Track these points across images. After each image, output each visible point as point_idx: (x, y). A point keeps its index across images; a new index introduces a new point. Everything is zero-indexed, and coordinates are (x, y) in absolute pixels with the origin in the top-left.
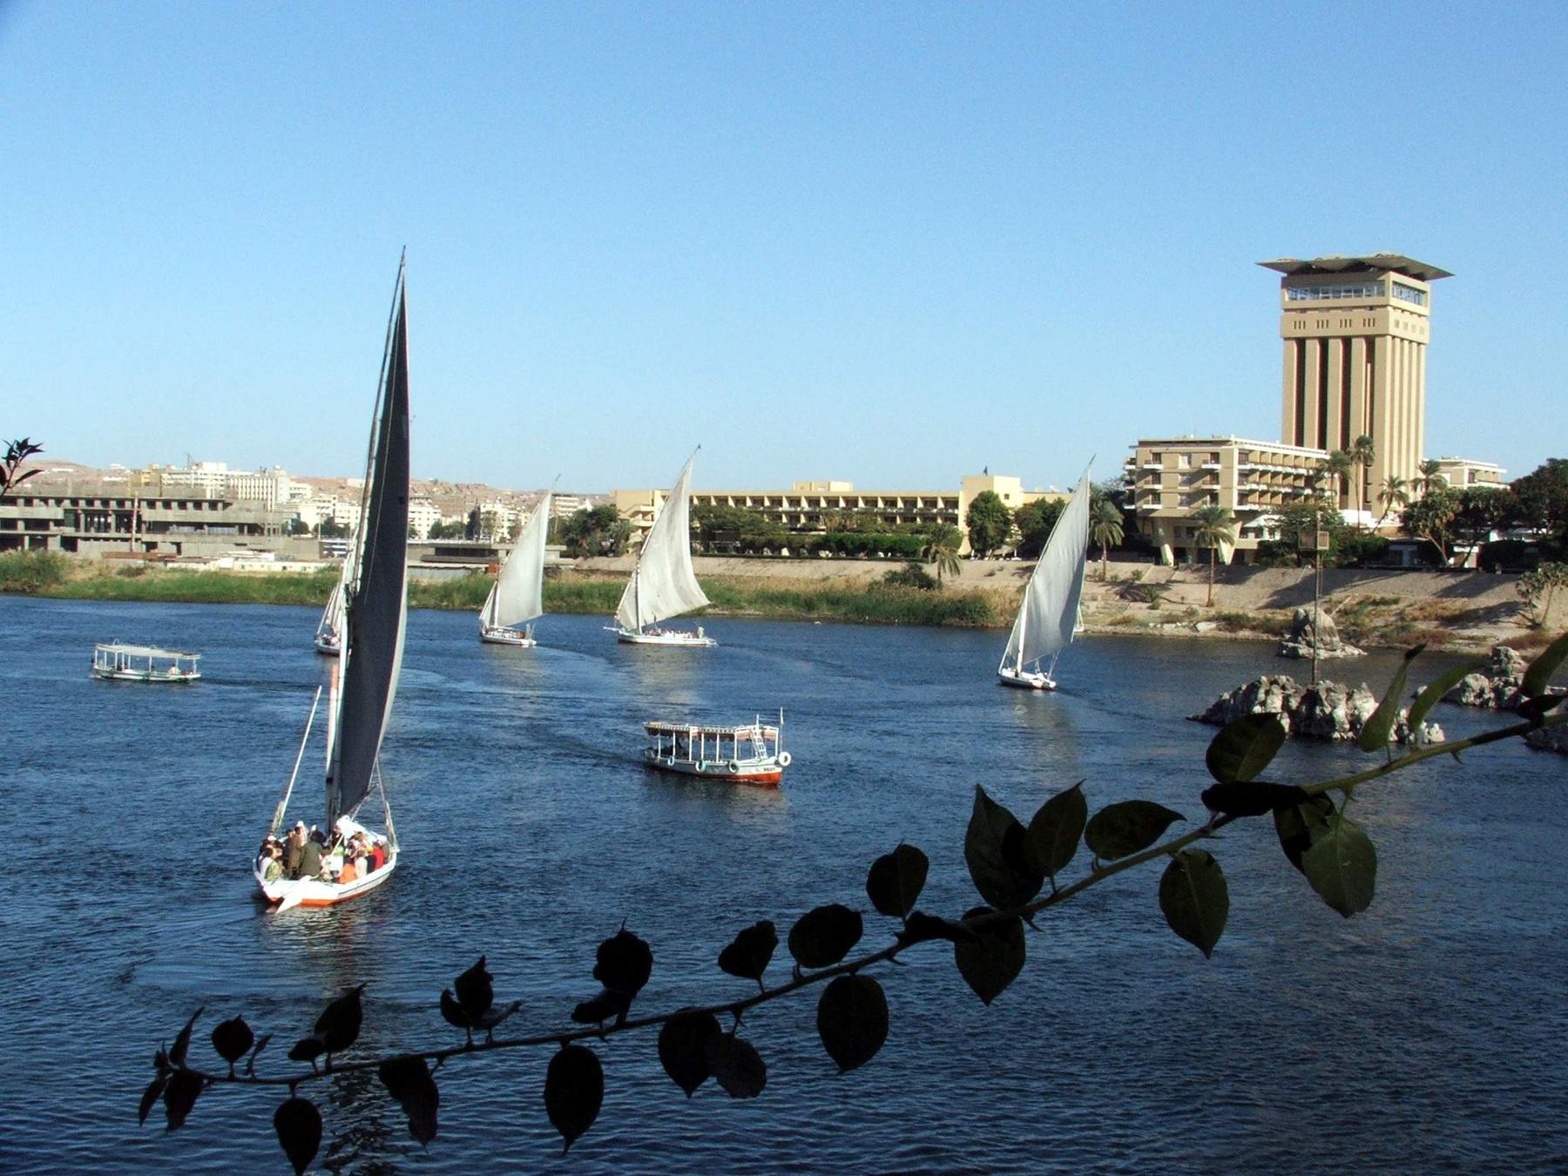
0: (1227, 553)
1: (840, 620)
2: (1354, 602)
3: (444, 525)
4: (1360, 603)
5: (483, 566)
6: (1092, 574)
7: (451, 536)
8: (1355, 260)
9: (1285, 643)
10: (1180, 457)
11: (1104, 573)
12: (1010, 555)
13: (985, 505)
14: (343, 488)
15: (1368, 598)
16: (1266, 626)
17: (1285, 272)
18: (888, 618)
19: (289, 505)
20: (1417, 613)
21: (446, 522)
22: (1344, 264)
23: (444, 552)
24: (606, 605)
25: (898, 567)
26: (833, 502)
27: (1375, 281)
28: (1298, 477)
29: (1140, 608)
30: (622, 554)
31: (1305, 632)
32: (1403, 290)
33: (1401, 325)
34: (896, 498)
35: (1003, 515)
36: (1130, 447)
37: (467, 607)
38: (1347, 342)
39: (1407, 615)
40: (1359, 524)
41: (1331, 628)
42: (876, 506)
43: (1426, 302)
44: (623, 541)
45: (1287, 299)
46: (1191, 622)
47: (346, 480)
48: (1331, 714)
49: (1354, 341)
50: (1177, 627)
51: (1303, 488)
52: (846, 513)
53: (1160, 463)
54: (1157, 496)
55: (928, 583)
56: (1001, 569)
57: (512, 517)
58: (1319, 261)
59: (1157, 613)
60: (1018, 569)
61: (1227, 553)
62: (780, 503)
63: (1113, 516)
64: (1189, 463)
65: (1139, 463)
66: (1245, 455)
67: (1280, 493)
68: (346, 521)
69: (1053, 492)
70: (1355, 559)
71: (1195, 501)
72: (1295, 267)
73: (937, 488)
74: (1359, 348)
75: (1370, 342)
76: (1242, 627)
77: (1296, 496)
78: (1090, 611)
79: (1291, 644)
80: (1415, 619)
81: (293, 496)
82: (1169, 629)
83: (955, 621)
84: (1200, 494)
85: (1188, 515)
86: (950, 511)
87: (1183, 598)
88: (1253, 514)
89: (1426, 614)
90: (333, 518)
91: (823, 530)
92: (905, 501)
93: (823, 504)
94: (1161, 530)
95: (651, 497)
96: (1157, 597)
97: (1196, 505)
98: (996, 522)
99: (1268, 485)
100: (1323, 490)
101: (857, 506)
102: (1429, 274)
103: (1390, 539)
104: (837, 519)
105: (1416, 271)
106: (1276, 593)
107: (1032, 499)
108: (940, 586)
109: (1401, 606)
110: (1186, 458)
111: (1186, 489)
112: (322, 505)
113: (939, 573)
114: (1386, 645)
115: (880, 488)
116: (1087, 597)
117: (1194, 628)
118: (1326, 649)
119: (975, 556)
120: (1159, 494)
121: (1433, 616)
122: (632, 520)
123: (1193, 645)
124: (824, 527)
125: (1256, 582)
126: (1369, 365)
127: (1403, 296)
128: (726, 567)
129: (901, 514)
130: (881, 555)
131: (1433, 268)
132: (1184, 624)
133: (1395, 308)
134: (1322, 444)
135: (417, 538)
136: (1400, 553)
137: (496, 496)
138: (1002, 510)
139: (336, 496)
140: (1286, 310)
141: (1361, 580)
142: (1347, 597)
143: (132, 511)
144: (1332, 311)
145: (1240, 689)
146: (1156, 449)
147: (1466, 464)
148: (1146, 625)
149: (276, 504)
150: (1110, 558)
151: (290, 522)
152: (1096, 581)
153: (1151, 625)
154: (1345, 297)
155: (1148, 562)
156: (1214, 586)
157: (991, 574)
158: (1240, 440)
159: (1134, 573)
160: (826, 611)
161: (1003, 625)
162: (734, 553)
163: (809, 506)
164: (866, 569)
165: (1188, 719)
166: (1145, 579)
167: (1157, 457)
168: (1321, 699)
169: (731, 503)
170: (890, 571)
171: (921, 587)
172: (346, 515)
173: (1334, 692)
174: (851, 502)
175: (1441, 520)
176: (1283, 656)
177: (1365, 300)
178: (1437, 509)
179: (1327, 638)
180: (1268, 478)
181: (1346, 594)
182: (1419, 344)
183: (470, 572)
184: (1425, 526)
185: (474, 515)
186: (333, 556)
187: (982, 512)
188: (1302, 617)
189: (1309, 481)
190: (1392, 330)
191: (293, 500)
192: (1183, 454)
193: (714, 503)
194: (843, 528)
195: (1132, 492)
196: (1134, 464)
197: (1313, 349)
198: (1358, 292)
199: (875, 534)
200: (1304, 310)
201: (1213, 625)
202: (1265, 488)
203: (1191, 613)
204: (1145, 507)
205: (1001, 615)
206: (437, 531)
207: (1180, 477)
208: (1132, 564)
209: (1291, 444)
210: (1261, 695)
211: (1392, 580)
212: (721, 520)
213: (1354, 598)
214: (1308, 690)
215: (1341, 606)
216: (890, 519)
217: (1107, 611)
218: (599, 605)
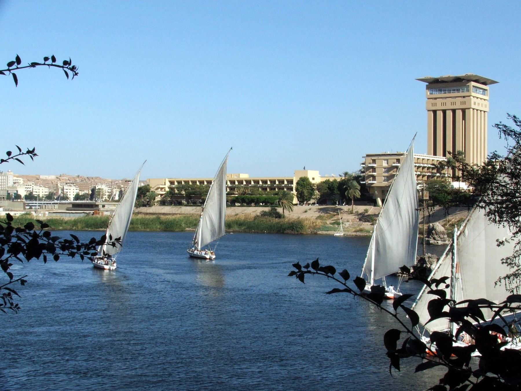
1: (242, 232)
2: (456, 221)
3: (80, 194)
4: (458, 221)
5: (92, 212)
6: (347, 210)
7: (83, 199)
8: (456, 77)
10: (384, 161)
11: (352, 210)
12: (314, 204)
13: (303, 182)
14: (38, 179)
18: (262, 231)
19: (13, 187)
21: (81, 193)
22: (432, 80)
23: (76, 206)
24: (143, 228)
25: (267, 209)
26: (241, 182)
27: (465, 85)
29: (367, 225)
30: (152, 205)
31: (432, 233)
33: (476, 104)
34: (196, 181)
35: (311, 187)
36: (363, 157)
37: (84, 229)
38: (454, 111)
40: (459, 188)
41: (443, 232)
42: (259, 184)
43: (487, 94)
44: (152, 200)
45: (428, 94)
47: (39, 176)
48: (430, 267)
49: (457, 111)
51: (436, 173)
52: (246, 187)
53: (375, 164)
54: (374, 178)
55: (279, 216)
56: (310, 209)
57: (109, 191)
58: (441, 78)
60: (317, 209)
62: (250, 183)
63: (355, 186)
64: (387, 163)
65: (367, 164)
67: (426, 175)
68: (38, 194)
69: (333, 177)
71: (390, 179)
72: (431, 81)
73: (285, 176)
74: (459, 114)
75: (464, 111)
77: (433, 176)
78: (346, 227)
79: (427, 239)
81: (15, 183)
83: (289, 231)
86: (290, 185)
90: (32, 193)
91: (237, 194)
92: (271, 181)
93: (237, 183)
94: (376, 192)
95: (164, 182)
100: (444, 174)
101: (243, 184)
102: (488, 82)
104: (242, 189)
105: (482, 81)
107: (324, 180)
108: (284, 217)
110: (386, 161)
111: (386, 174)
112: (27, 187)
113: (283, 212)
115: (261, 176)
116: (345, 220)
118: (441, 241)
119: (299, 204)
122: (156, 191)
124: (237, 193)
126: (464, 121)
127: (478, 92)
128: (196, 210)
129: (269, 187)
130: (261, 204)
131: (490, 80)
133: (474, 97)
134: (444, 155)
135: (69, 200)
137: (102, 181)
138: (310, 184)
139: (34, 183)
140: (428, 99)
141: (459, 211)
142: (453, 219)
144: (447, 99)
146: (374, 158)
149: (7, 187)
150: (356, 204)
151: (13, 194)
152: (349, 214)
154: (453, 92)
155: (371, 205)
157: (306, 212)
159: (365, 210)
160: (236, 228)
161: (310, 233)
162: (200, 205)
163: (231, 184)
164: (254, 210)
166: (370, 213)
167: (374, 161)
168: (426, 261)
169: (198, 183)
170: (263, 211)
171: (276, 217)
172: (38, 191)
173: (431, 258)
174: (248, 182)
177: (461, 94)
179: (442, 236)
180: (421, 169)
181: (453, 217)
182: (484, 112)
183: (86, 214)
185: (93, 190)
186: (32, 208)
187: (302, 185)
188: (431, 227)
190: (473, 106)
191: (15, 185)
192: (385, 160)
193: (191, 183)
194: (244, 193)
195: (364, 176)
197: (440, 115)
198: (458, 90)
199: (258, 196)
200: (436, 99)
202: (419, 173)
205: (309, 228)
206: (77, 197)
207: (384, 170)
208: (365, 206)
209: (441, 156)
212: (193, 191)
213: (456, 219)
214: (421, 258)
215: (450, 222)
216: (265, 189)
217: (353, 226)
218: (140, 227)
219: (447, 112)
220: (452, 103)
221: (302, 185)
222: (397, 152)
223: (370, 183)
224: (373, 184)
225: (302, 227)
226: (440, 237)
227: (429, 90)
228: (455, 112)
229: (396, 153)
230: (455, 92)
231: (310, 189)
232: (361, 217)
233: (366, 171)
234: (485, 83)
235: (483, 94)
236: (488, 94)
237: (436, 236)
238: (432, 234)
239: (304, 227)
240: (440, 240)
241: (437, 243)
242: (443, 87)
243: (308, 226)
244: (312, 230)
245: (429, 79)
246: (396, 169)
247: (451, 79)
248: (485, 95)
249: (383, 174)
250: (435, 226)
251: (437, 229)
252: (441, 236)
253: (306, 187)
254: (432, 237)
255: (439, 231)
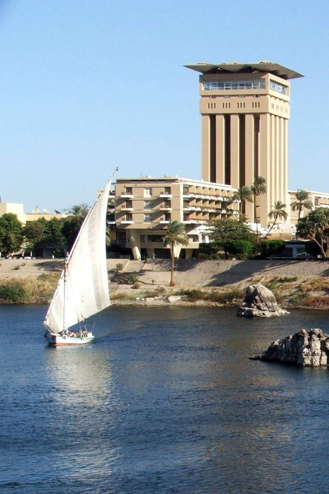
0: (176, 252)
2: (267, 281)
4: (271, 281)
8: (246, 65)
9: (243, 308)
10: (145, 190)
15: (276, 278)
16: (213, 297)
17: (201, 72)
20: (309, 286)
22: (241, 67)
27: (260, 79)
28: (217, 202)
31: (256, 300)
32: (275, 85)
39: (304, 288)
45: (203, 89)
46: (164, 296)
50: (155, 299)
51: (221, 210)
53: (132, 194)
56: (24, 265)
59: (138, 291)
61: (176, 252)
64: (151, 194)
66: (187, 188)
70: (260, 254)
72: (208, 69)
74: (250, 121)
76: (199, 298)
79: (247, 309)
80: (309, 290)
82: (150, 301)
84: (158, 214)
85: (151, 228)
87: (153, 281)
88: (192, 226)
89: (316, 287)
94: (132, 238)
96: (137, 280)
97: (155, 221)
98: (16, 234)
99: (202, 208)
102: (289, 76)
103: (286, 241)
106: (215, 276)
109: (298, 282)
110: (148, 191)
111: (149, 211)
114: (294, 307)
117: (167, 300)
120: (131, 214)
121: (320, 288)
123: (166, 310)
125: (200, 269)
131: (294, 71)
132: (160, 297)
133: (271, 96)
134: (228, 181)
136: (291, 249)
140: (203, 96)
141: (271, 266)
142: (262, 278)
143: (257, 239)
144: (246, 97)
145: (288, 338)
146: (129, 185)
147: (313, 193)
148: (135, 299)
153: (138, 299)
155: (125, 258)
156: (174, 272)
157: (17, 269)
158: (184, 180)
159: (118, 266)
161: (35, 302)
165: (251, 359)
166: (125, 270)
175: (322, 228)
176: (242, 316)
177: (252, 91)
178: (319, 222)
179: (270, 304)
180: (200, 203)
181: (262, 275)
182: (285, 119)
184: (313, 232)
187: (6, 227)
188: (252, 291)
189: (224, 204)
190: (270, 110)
192: (146, 188)
196: (114, 195)
197: (221, 121)
198: (248, 86)
200: (214, 97)
201: (179, 298)
203: (162, 290)
204: (123, 222)
205: (33, 295)
207: (145, 203)
210: (306, 342)
211: (291, 266)
213: (267, 278)
219: (232, 118)
220: (240, 104)
221: (6, 227)
222: (165, 177)
223: (162, 224)
224: (128, 225)
225: (22, 292)
226: (267, 305)
227: (203, 83)
228: (215, 117)
229: (164, 179)
230: (244, 88)
231: (19, 233)
232: (114, 277)
233: (117, 206)
234: (284, 77)
235: (283, 92)
236: (289, 94)
237: (261, 305)
238: (254, 302)
239: (25, 293)
240: (267, 309)
241: (264, 314)
242: (226, 80)
243: (31, 291)
244: (37, 297)
245: (204, 66)
246: (164, 202)
247: (237, 69)
248: (285, 94)
249: (145, 210)
250: (258, 288)
251: (262, 293)
252: (268, 304)
253: (14, 230)
254: (255, 305)
255: (265, 296)
